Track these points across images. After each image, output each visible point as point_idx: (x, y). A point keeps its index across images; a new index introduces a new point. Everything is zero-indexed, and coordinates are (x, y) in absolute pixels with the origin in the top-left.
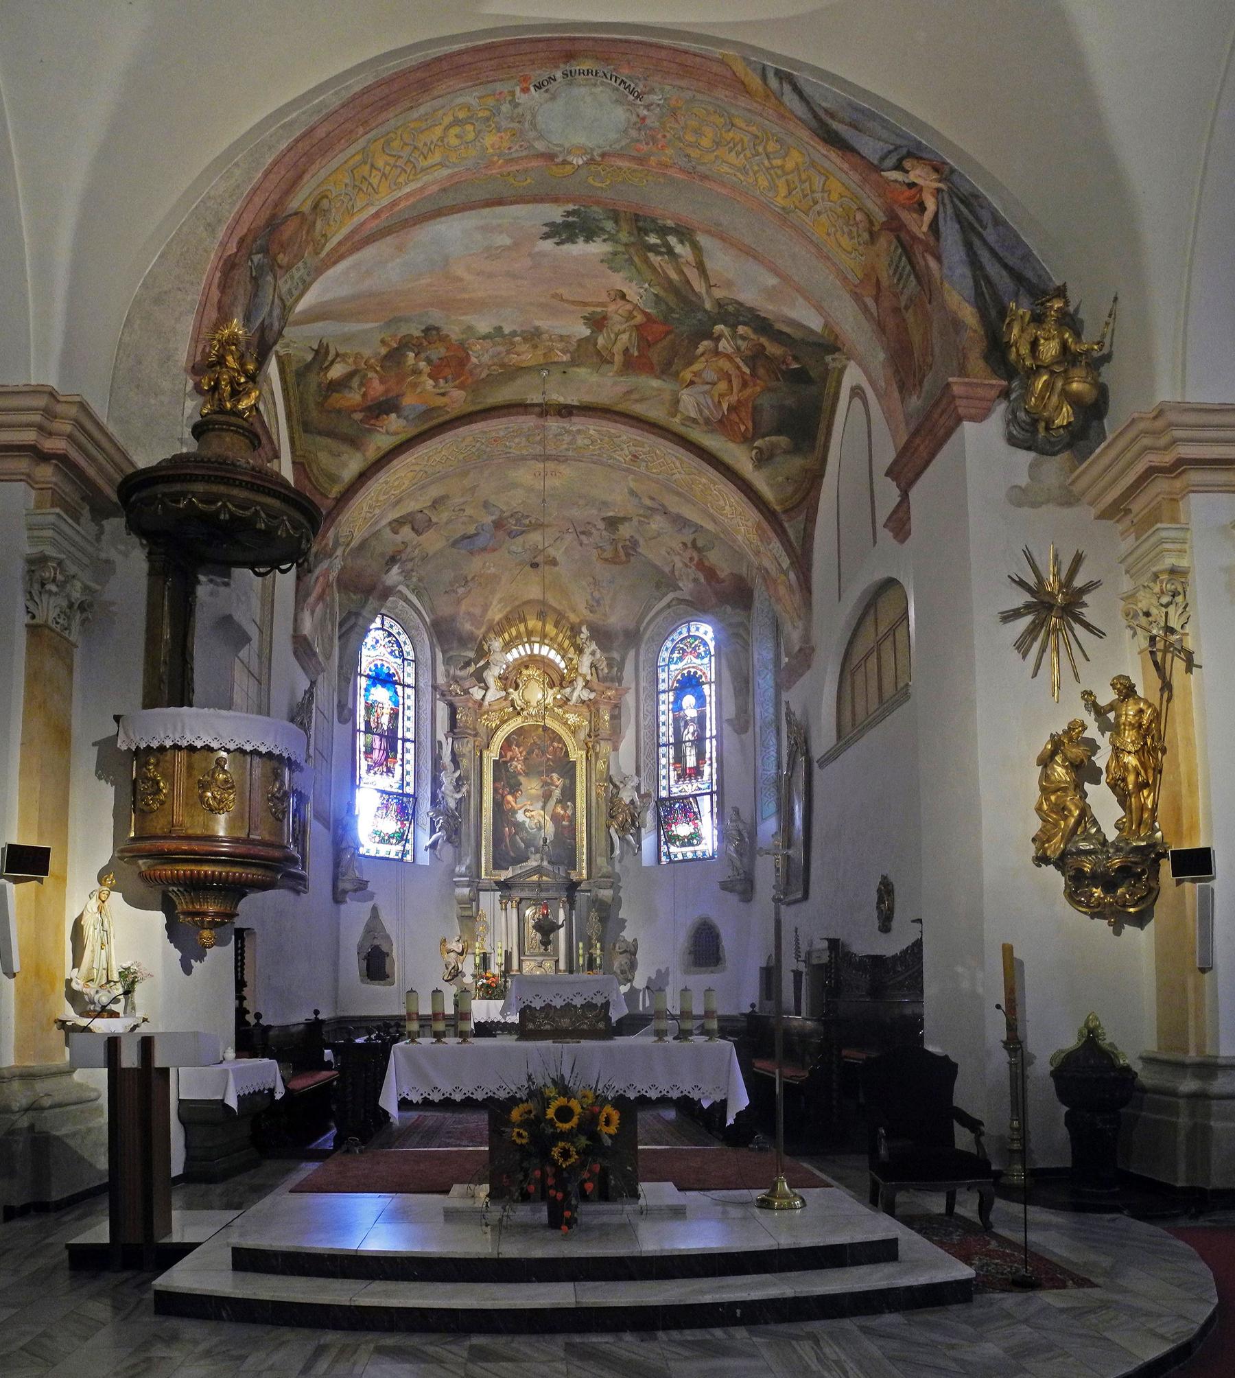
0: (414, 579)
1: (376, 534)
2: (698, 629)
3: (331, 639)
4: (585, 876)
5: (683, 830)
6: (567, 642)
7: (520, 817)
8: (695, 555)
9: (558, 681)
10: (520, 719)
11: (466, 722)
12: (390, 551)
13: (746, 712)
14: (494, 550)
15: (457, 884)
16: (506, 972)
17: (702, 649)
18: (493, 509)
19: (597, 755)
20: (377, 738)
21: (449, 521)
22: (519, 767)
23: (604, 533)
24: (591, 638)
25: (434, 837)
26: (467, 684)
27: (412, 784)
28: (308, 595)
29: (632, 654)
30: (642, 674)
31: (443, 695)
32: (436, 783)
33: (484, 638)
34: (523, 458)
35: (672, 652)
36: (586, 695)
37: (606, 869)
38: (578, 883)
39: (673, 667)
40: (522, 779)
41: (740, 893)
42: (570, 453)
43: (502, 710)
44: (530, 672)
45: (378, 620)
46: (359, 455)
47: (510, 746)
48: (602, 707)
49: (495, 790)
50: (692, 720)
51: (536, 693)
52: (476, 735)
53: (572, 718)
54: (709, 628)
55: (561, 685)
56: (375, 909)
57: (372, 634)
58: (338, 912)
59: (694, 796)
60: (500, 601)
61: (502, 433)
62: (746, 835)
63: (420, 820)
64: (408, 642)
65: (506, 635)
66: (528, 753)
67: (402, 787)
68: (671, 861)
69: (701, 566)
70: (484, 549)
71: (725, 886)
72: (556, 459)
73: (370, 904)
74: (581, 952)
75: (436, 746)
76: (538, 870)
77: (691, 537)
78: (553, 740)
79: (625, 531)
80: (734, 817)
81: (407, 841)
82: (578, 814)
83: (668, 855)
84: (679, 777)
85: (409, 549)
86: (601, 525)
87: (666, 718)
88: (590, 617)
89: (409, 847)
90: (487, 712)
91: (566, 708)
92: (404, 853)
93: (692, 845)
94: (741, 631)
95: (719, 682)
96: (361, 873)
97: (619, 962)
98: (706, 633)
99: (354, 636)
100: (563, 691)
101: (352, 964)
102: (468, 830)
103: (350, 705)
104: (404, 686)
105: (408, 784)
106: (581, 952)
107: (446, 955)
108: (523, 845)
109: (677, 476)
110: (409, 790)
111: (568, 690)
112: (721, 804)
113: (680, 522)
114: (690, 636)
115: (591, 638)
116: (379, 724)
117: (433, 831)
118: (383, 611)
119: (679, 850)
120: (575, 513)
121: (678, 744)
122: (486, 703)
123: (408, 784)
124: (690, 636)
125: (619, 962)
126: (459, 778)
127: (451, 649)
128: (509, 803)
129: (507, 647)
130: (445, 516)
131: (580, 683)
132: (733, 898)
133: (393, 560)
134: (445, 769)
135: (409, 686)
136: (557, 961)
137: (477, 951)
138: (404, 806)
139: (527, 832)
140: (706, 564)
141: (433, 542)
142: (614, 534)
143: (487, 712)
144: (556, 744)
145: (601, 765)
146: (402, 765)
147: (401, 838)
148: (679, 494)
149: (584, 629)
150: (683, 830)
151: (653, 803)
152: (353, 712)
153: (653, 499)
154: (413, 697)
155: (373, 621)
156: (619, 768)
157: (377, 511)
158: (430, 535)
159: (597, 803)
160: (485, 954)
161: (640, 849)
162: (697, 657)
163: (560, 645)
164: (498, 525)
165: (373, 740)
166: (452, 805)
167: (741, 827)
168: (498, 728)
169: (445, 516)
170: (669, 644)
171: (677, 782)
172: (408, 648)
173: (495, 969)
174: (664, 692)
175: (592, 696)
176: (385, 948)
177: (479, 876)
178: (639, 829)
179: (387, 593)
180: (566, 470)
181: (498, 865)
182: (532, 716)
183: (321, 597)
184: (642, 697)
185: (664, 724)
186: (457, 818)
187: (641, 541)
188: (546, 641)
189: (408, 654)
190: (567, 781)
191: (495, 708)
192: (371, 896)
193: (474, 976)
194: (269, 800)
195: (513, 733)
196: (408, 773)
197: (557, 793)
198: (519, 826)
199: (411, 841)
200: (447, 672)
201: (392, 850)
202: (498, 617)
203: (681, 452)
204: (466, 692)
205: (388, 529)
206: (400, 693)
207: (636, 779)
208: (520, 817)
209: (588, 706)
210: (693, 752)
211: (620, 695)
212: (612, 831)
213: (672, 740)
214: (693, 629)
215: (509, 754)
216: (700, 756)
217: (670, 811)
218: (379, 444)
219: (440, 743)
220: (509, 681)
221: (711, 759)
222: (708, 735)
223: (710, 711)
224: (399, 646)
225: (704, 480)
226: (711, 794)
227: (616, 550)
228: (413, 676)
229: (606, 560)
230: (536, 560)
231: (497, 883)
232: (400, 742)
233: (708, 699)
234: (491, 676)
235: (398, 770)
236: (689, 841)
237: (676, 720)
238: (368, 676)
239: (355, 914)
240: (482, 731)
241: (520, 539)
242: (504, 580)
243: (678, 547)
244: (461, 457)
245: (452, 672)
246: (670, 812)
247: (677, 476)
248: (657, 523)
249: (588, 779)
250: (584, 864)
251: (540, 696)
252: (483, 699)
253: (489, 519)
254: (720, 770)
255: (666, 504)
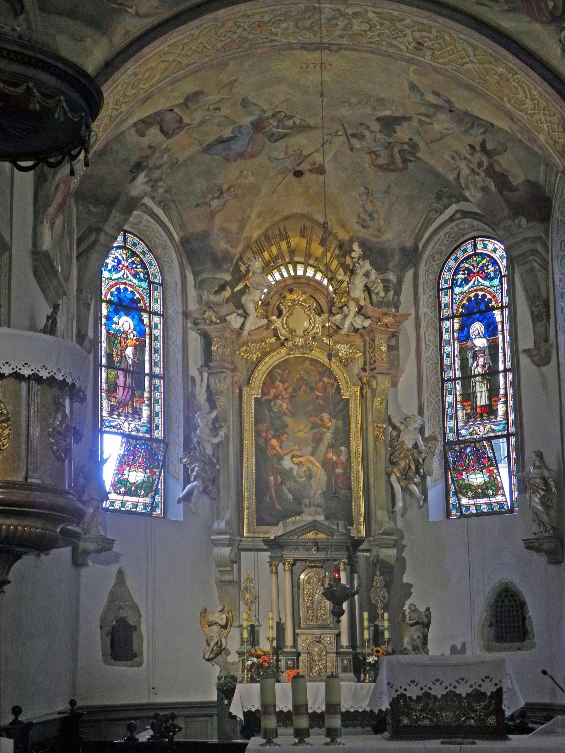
0: (161, 190)
1: (119, 137)
2: (485, 247)
3: (70, 258)
4: (363, 533)
5: (477, 479)
6: (335, 263)
7: (287, 463)
8: (484, 159)
9: (329, 307)
10: (284, 351)
11: (223, 354)
12: (134, 159)
13: (546, 340)
14: (253, 157)
15: (215, 543)
16: (278, 650)
17: (491, 269)
18: (253, 108)
19: (373, 391)
20: (121, 374)
21: (203, 122)
22: (285, 406)
23: (379, 136)
24: (364, 257)
25: (188, 487)
26: (223, 311)
27: (161, 428)
28: (47, 205)
29: (410, 274)
30: (423, 298)
31: (196, 323)
32: (190, 425)
33: (241, 259)
34: (290, 47)
35: (456, 273)
36: (360, 322)
37: (388, 525)
38: (360, 542)
39: (457, 290)
40: (288, 420)
41: (548, 553)
42: (344, 41)
43: (263, 340)
44: (295, 296)
45: (120, 238)
46: (104, 40)
47: (273, 382)
48: (378, 336)
49: (258, 434)
50: (482, 350)
51: (304, 322)
52: (234, 370)
53: (343, 350)
54: (500, 246)
55: (331, 313)
56: (120, 573)
57: (115, 253)
58: (79, 575)
59: (489, 439)
60: (259, 215)
61: (267, 18)
62: (552, 484)
63: (171, 468)
64: (154, 262)
65: (266, 254)
66: (295, 390)
67: (150, 431)
68: (462, 516)
69: (491, 172)
70: (241, 155)
71: (530, 545)
72: (329, 47)
73: (114, 569)
74: (366, 623)
75: (189, 382)
76: (313, 526)
77: (481, 138)
78: (322, 375)
79: (403, 132)
80: (537, 463)
81: (157, 492)
82: (353, 461)
83: (459, 507)
84: (469, 416)
85: (157, 155)
86: (376, 127)
87: (452, 348)
88: (363, 233)
89: (158, 498)
90: (246, 343)
91: (336, 337)
92: (154, 506)
93: (486, 496)
94: (539, 248)
95: (512, 306)
96: (105, 530)
97: (410, 636)
98: (495, 250)
99: (94, 255)
100: (332, 319)
101: (93, 640)
102: (227, 479)
103: (91, 334)
104: (151, 313)
105: (157, 427)
106: (366, 623)
107: (207, 629)
108: (290, 496)
109: (469, 66)
110: (158, 434)
111: (339, 317)
112: (520, 448)
113: (468, 120)
114: (476, 254)
115: (364, 257)
116: (123, 357)
117: (187, 481)
118: (126, 227)
119: (472, 502)
120: (344, 112)
121: (467, 378)
122: (245, 332)
123: (157, 427)
124: (476, 254)
125: (410, 636)
126: (216, 420)
127: (202, 271)
128: (273, 448)
129: (268, 268)
130: (198, 116)
131: (353, 308)
132: (540, 559)
133: (138, 167)
134: (200, 409)
135: (156, 314)
136: (338, 635)
137: (245, 624)
138: (143, 450)
139: (295, 481)
140: (498, 169)
141: (183, 146)
142: (390, 135)
143: (246, 343)
144: (326, 380)
145: (378, 403)
146: (150, 406)
147: (148, 487)
148: (469, 87)
149: (356, 247)
150: (477, 479)
151: (440, 447)
152: (96, 341)
153: (437, 94)
154: (161, 326)
155: (115, 239)
156: (398, 406)
157: (124, 108)
158: (180, 138)
159: (376, 446)
160: (252, 626)
161: (426, 500)
162: (485, 278)
163: (327, 266)
164: (258, 126)
165: (117, 376)
166: (209, 451)
167: (546, 474)
168: (259, 361)
169: (198, 116)
170: (452, 263)
171: (466, 423)
172: (154, 270)
173: (265, 646)
174: (447, 318)
175: (367, 323)
176: (132, 621)
177: (241, 534)
178: (424, 477)
179: (133, 204)
180: (335, 60)
181: (260, 522)
182: (297, 346)
183: (61, 208)
184: (423, 324)
185: (448, 355)
186: (214, 465)
187: (422, 145)
188: (311, 262)
189: (155, 276)
190: (340, 423)
191: (253, 338)
192: (117, 558)
193: (240, 654)
194: (50, 436)
195: (276, 367)
196: (157, 414)
197: (329, 436)
198: (286, 474)
199: (162, 492)
200: (200, 297)
201: (140, 502)
202: (256, 234)
203: (475, 37)
204: (223, 320)
205: (133, 131)
206: (146, 321)
207: (419, 419)
208: (287, 463)
209: (362, 335)
210: (484, 388)
211: (399, 321)
212: (393, 479)
213: (458, 374)
214: (480, 246)
215: (273, 391)
216: (493, 392)
217: (460, 456)
218: (128, 28)
219: (193, 379)
220: (272, 308)
221: (506, 395)
222: (501, 367)
223: (503, 339)
224: (144, 267)
225: (501, 70)
226: (508, 436)
227: (392, 157)
228: (160, 301)
229: (380, 167)
230: (300, 168)
231: (266, 541)
232: (147, 378)
233: (500, 327)
234: (253, 300)
235: (145, 412)
236: (481, 492)
237: (462, 350)
238: (109, 302)
239: (98, 580)
240: (242, 366)
241: (281, 144)
242: (263, 191)
243: (465, 151)
244: (219, 46)
245: (205, 297)
246: (460, 458)
247: (469, 66)
248: (442, 123)
249: (364, 419)
250: (362, 519)
251: (306, 324)
252: (242, 327)
253: (248, 120)
254: (518, 409)
255: (452, 99)
